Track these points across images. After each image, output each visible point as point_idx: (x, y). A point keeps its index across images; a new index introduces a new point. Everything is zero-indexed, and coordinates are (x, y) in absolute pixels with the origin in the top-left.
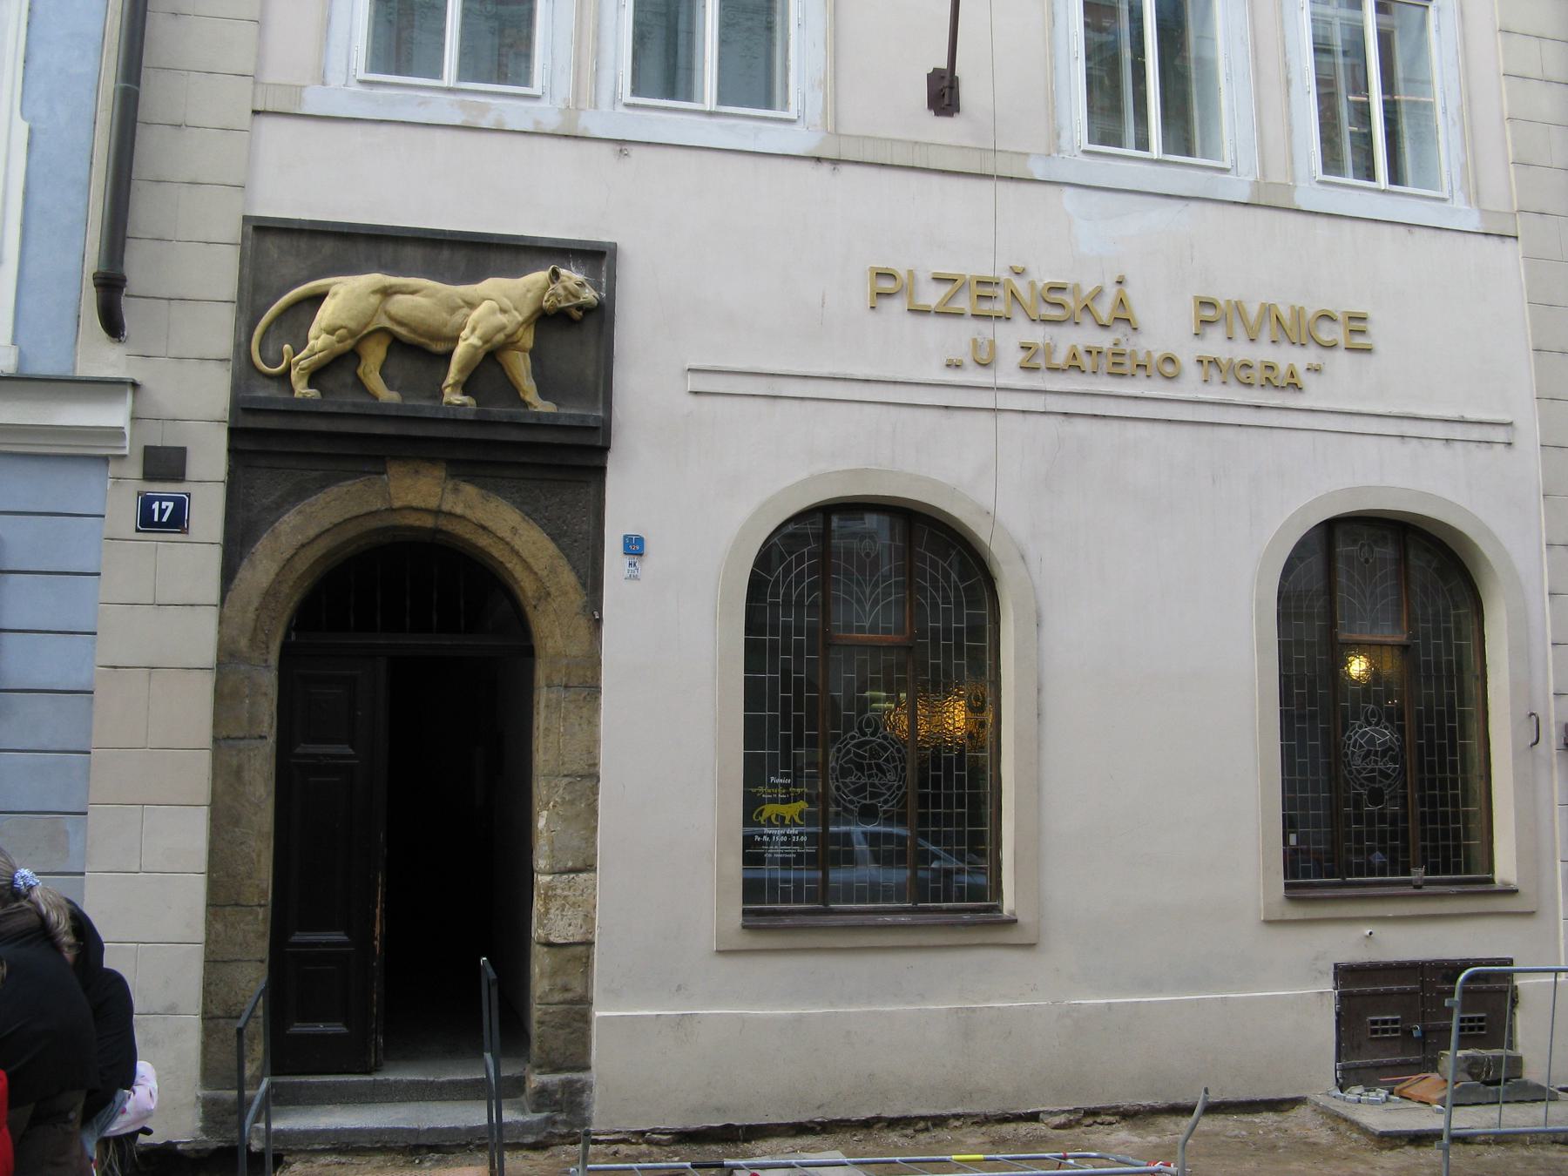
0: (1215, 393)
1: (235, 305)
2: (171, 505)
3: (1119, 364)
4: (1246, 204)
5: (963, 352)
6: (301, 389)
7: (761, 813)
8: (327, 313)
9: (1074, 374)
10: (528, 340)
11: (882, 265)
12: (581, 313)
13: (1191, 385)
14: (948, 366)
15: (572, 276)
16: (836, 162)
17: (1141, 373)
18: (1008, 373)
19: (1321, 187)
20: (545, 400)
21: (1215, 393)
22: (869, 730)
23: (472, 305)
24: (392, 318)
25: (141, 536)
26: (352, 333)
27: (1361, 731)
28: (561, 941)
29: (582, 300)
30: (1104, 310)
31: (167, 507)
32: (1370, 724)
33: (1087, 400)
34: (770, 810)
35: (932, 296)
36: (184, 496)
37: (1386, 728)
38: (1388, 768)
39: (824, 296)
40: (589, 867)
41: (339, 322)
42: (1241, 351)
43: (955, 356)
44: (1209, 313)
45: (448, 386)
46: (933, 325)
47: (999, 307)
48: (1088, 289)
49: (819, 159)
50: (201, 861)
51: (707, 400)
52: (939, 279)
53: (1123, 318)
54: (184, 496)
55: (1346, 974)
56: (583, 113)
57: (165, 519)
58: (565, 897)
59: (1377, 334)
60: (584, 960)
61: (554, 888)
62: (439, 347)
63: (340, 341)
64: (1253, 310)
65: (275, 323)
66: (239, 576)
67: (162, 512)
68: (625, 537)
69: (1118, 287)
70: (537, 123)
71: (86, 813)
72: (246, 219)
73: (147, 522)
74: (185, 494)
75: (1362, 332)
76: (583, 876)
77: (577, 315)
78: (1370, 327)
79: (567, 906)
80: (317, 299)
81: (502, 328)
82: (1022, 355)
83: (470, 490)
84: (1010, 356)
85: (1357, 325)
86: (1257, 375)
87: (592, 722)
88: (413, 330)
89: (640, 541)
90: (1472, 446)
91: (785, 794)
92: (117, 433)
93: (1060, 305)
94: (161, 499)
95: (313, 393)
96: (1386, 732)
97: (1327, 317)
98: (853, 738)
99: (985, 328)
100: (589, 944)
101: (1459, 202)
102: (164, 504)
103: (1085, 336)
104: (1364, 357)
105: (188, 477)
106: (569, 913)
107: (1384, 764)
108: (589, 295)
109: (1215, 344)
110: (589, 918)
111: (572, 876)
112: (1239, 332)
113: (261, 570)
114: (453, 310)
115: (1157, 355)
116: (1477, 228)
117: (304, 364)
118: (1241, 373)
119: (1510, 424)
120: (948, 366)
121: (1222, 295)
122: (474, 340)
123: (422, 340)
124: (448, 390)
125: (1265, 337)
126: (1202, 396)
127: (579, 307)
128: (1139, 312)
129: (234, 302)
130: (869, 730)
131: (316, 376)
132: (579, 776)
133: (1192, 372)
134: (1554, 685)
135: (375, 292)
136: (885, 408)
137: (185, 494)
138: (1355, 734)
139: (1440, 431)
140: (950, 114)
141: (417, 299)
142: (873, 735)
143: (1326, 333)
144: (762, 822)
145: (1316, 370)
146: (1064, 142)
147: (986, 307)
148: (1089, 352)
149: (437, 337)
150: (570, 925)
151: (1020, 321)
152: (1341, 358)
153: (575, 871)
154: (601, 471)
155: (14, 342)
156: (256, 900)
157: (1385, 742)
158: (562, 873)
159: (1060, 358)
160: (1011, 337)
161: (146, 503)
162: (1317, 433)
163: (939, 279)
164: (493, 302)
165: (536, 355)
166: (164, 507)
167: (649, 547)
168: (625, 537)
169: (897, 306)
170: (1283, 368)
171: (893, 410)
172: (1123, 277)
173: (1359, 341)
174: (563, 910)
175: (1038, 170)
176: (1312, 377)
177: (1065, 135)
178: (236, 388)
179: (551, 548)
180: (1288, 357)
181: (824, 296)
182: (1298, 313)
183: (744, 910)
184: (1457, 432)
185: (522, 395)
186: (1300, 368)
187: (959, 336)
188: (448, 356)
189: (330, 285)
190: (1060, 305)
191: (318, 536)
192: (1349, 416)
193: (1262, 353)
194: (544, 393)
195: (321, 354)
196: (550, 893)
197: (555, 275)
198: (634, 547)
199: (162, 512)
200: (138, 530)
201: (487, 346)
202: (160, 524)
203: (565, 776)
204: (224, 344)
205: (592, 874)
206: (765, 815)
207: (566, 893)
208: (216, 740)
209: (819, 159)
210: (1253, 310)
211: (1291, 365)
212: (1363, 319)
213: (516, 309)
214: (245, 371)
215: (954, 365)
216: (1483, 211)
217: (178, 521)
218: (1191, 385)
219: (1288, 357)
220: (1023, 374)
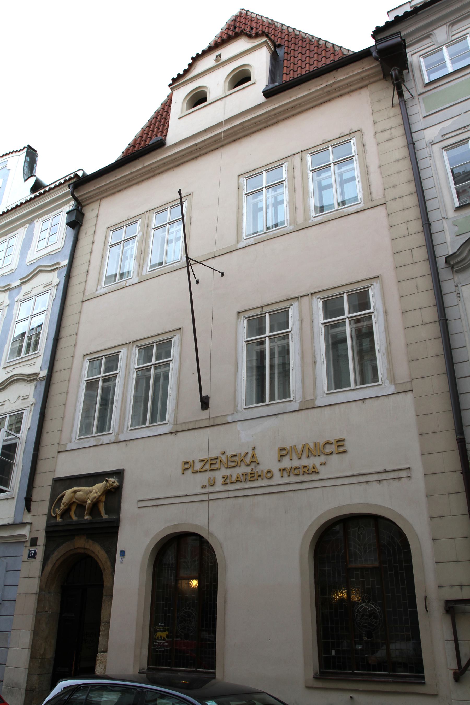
0: (286, 480)
2: (33, 552)
3: (252, 477)
4: (298, 410)
5: (206, 482)
6: (59, 520)
7: (156, 635)
8: (65, 500)
9: (238, 483)
12: (114, 490)
14: (202, 487)
15: (111, 480)
16: (177, 432)
17: (260, 478)
18: (219, 487)
19: (328, 395)
20: (106, 515)
21: (286, 480)
22: (188, 608)
23: (91, 492)
25: (28, 560)
26: (67, 504)
27: (360, 606)
30: (248, 459)
32: (365, 602)
33: (242, 491)
34: (159, 634)
37: (373, 604)
38: (373, 622)
39: (171, 473)
41: (65, 502)
42: (296, 463)
43: (204, 484)
46: (199, 475)
48: (243, 454)
49: (172, 433)
51: (142, 509)
52: (201, 461)
53: (254, 461)
56: (120, 435)
58: (101, 660)
59: (348, 445)
63: (65, 506)
64: (300, 447)
66: (45, 569)
67: (32, 554)
70: (110, 440)
71: (11, 632)
75: (343, 445)
77: (113, 490)
78: (346, 443)
81: (95, 497)
82: (223, 480)
83: (91, 542)
84: (220, 481)
85: (340, 442)
86: (301, 471)
88: (79, 501)
89: (124, 552)
90: (391, 481)
91: (163, 629)
92: (24, 536)
93: (234, 461)
96: (373, 606)
97: (327, 443)
98: (183, 610)
99: (211, 474)
102: (33, 552)
103: (244, 469)
104: (343, 455)
105: (38, 545)
107: (371, 620)
109: (286, 463)
111: (103, 653)
112: (295, 457)
113: (49, 567)
115: (265, 471)
116: (393, 392)
117: (59, 513)
118: (294, 471)
120: (202, 487)
123: (81, 503)
125: (305, 455)
126: (280, 482)
127: (113, 488)
128: (259, 457)
130: (188, 608)
131: (62, 516)
133: (277, 474)
134: (425, 64)
135: (72, 493)
136: (184, 504)
138: (358, 607)
139: (376, 477)
140: (201, 409)
141: (81, 493)
142: (189, 609)
143: (328, 449)
144: (156, 638)
145: (323, 464)
146: (239, 408)
147: (213, 467)
150: (101, 669)
151: (223, 469)
154: (117, 533)
155: (14, 516)
157: (371, 610)
159: (234, 479)
160: (219, 475)
162: (323, 488)
165: (105, 503)
167: (126, 553)
168: (121, 551)
169: (189, 471)
170: (311, 466)
171: (187, 504)
173: (341, 449)
175: (230, 419)
176: (323, 467)
177: (239, 405)
178: (48, 521)
179: (106, 555)
181: (171, 473)
184: (384, 476)
186: (318, 465)
187: (203, 478)
189: (66, 492)
190: (234, 461)
191: (61, 557)
192: (336, 479)
193: (305, 461)
194: (106, 513)
197: (107, 481)
198: (123, 554)
199: (32, 554)
200: (28, 559)
201: (92, 503)
203: (104, 622)
204: (46, 511)
206: (157, 636)
207: (101, 659)
208: (37, 612)
209: (172, 433)
211: (314, 464)
212: (343, 440)
213: (99, 492)
214: (49, 517)
215: (203, 487)
217: (34, 556)
218: (277, 479)
220: (223, 486)
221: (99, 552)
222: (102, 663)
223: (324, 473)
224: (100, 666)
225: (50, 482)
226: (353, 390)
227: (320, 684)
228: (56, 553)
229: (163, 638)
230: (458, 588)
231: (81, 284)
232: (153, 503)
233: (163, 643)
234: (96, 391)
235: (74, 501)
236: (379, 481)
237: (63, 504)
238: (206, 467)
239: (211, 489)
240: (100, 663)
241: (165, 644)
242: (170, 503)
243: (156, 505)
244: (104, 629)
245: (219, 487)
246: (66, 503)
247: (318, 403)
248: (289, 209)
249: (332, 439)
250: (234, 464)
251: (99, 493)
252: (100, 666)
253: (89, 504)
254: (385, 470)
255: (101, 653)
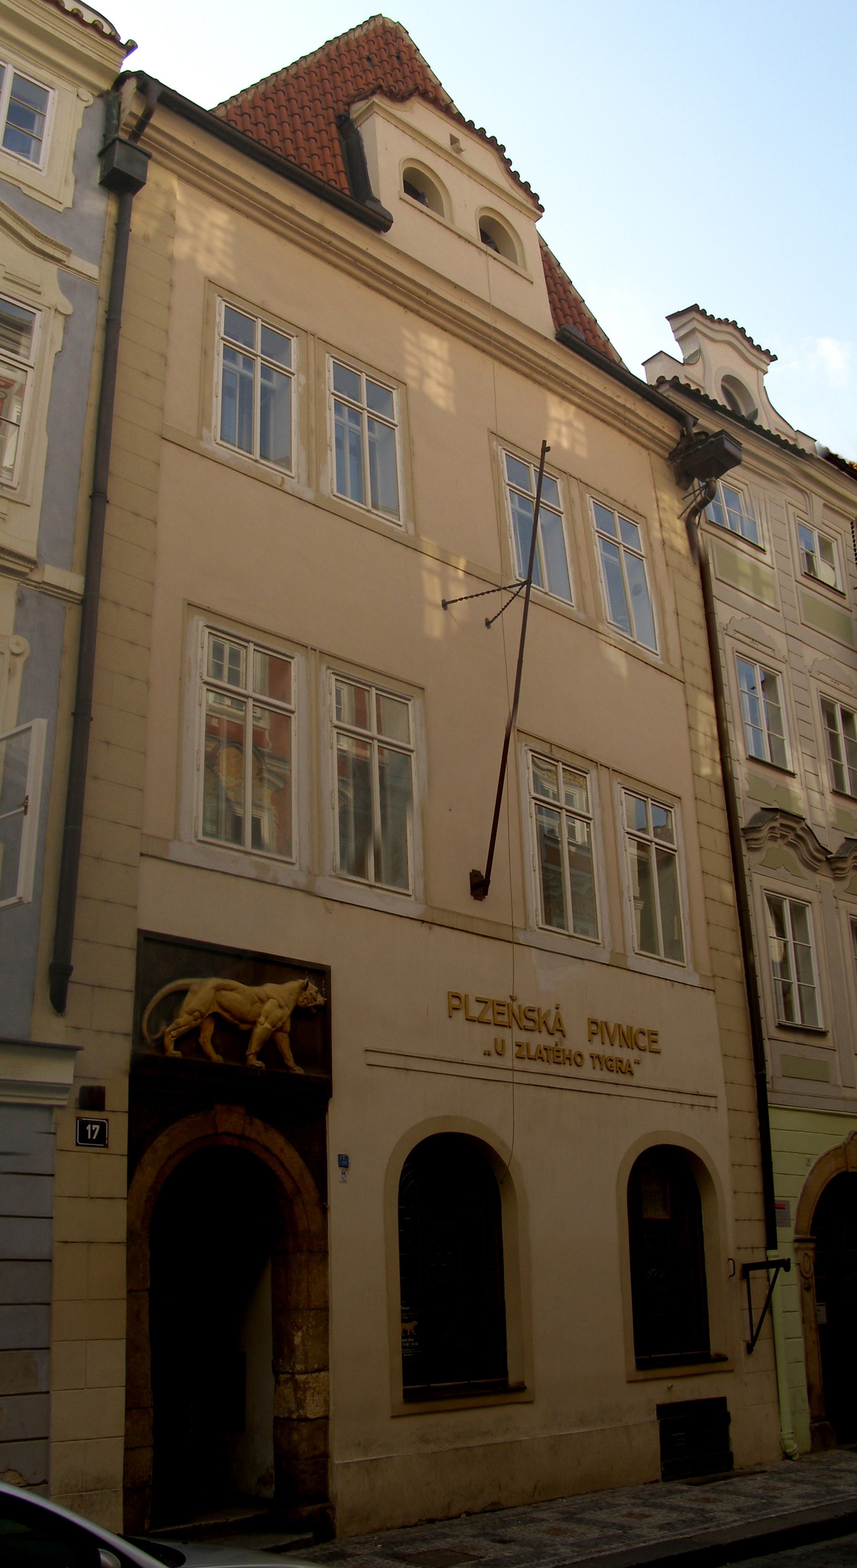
1: (133, 993)
2: (98, 1127)
4: (608, 965)
10: (288, 1027)
11: (454, 990)
13: (587, 1070)
18: (509, 1060)
23: (262, 1001)
24: (221, 1006)
25: (79, 1148)
28: (312, 1417)
29: (318, 1002)
31: (96, 1129)
35: (476, 1010)
36: (105, 1121)
40: (325, 1368)
44: (596, 1027)
45: (252, 1054)
47: (504, 1019)
49: (423, 922)
50: (122, 1379)
52: (479, 1001)
54: (105, 1121)
55: (665, 1412)
57: (94, 1137)
58: (314, 1388)
59: (663, 1043)
60: (324, 1429)
61: (308, 1383)
62: (244, 1027)
65: (484, 874)
67: (93, 1132)
68: (339, 1155)
69: (557, 1011)
72: (140, 932)
73: (83, 1138)
74: (106, 1120)
75: (656, 1042)
76: (322, 1373)
79: (315, 1394)
80: (182, 993)
84: (511, 1050)
87: (324, 1273)
88: (233, 1015)
89: (347, 1158)
94: (93, 1123)
95: (178, 1054)
100: (326, 1417)
101: (691, 967)
102: (94, 1127)
105: (107, 1108)
106: (316, 1398)
108: (320, 1000)
109: (597, 1048)
110: (327, 1402)
111: (317, 1374)
113: (148, 1175)
114: (253, 1003)
119: (716, 1097)
121: (599, 1018)
122: (267, 1025)
123: (237, 1022)
124: (251, 1057)
127: (316, 1007)
128: (567, 1028)
129: (132, 992)
131: (179, 1042)
132: (320, 1309)
133: (588, 1061)
137: (106, 1120)
139: (688, 1099)
145: (637, 1063)
148: (546, 1049)
149: (244, 1021)
150: (317, 1406)
152: (647, 1056)
153: (319, 1370)
156: (149, 1403)
158: (312, 1372)
161: (83, 1125)
163: (479, 1001)
164: (275, 1001)
165: (292, 1035)
166: (94, 1129)
167: (351, 1161)
168: (339, 1155)
169: (460, 1015)
172: (557, 1005)
174: (313, 1396)
180: (628, 1055)
182: (630, 1029)
183: (405, 1391)
184: (697, 1100)
185: (286, 1061)
187: (486, 1035)
188: (250, 1033)
194: (297, 1062)
195: (183, 1028)
196: (307, 1386)
198: (344, 1161)
199: (93, 1132)
200: (77, 1145)
202: (91, 1141)
205: (327, 1372)
207: (314, 1385)
208: (129, 1291)
209: (423, 922)
210: (612, 1027)
213: (287, 1006)
214: (138, 1037)
215: (487, 1054)
216: (701, 975)
217: (102, 1139)
219: (628, 1055)
221: (282, 1150)
222: (318, 1394)
223: (640, 1076)
224: (313, 1400)
225: (131, 940)
226: (371, 886)
227: (641, 1375)
228: (162, 1141)
229: (409, 1334)
230: (750, 1250)
231: (679, 613)
232: (400, 1062)
233: (410, 1342)
234: (388, 770)
235: (215, 1011)
236: (692, 1105)
237: (190, 1013)
238: (489, 1017)
239: (494, 1060)
240: (313, 1394)
241: (413, 1344)
242: (570, 1088)
243: (405, 1069)
244: (314, 1323)
245: (509, 1060)
246: (201, 1013)
247: (176, 852)
248: (212, 379)
249: (646, 1027)
250: (530, 1024)
251: (287, 1008)
252: (313, 1400)
253: (266, 1028)
254: (698, 1092)
255: (313, 1375)
